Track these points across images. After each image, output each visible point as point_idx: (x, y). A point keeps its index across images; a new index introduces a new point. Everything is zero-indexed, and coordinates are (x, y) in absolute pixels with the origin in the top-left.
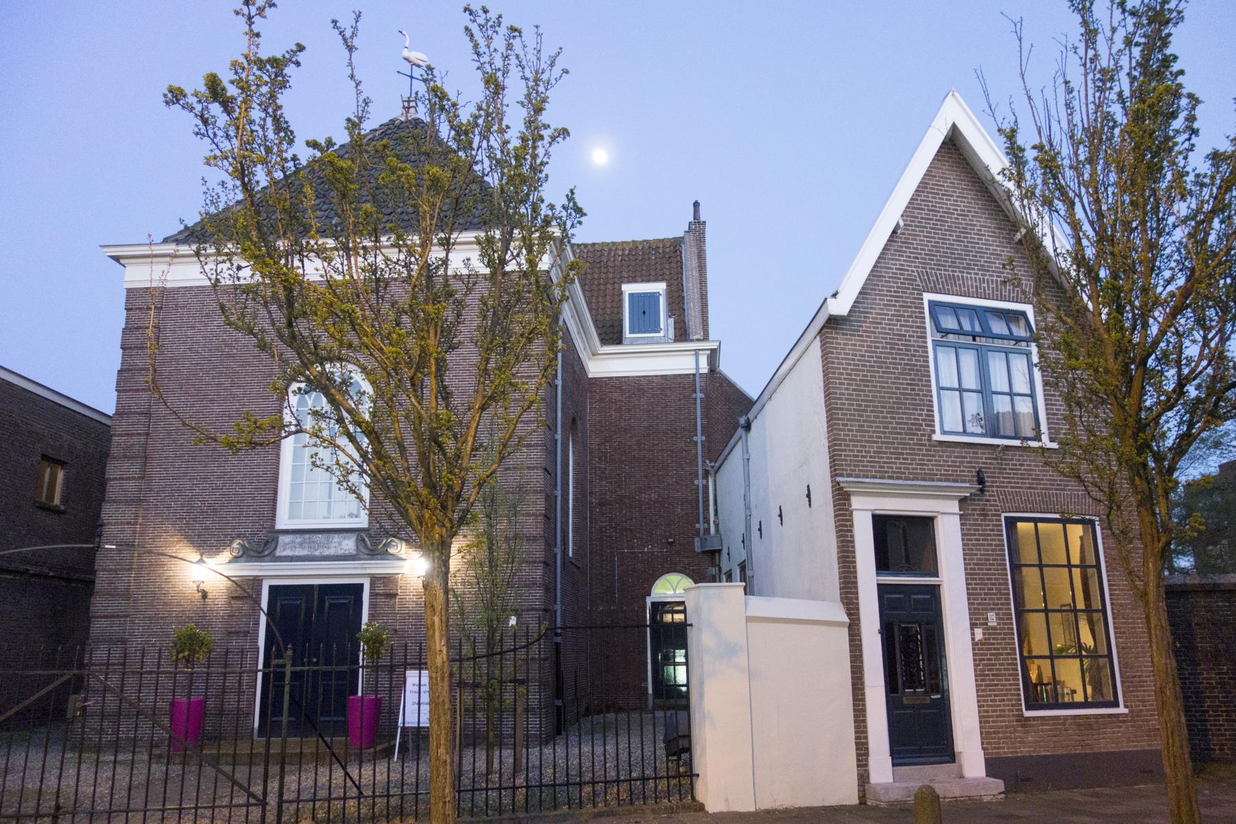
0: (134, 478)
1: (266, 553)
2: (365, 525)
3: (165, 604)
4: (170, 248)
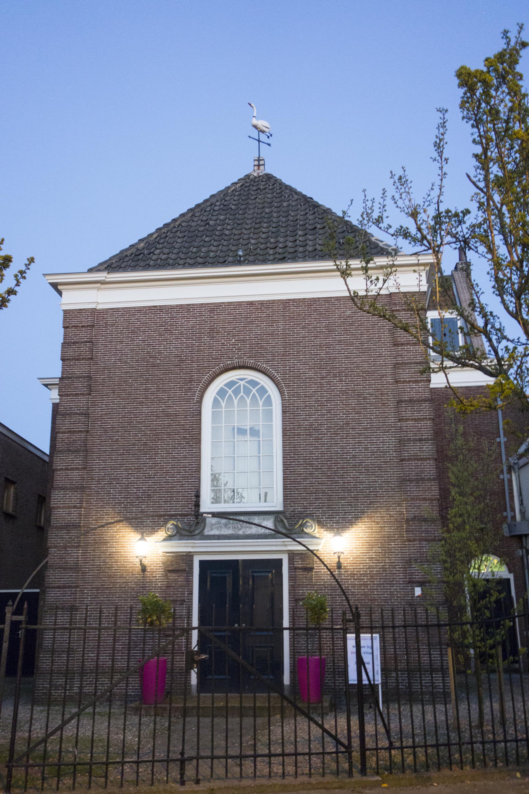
0: (77, 469)
1: (197, 532)
2: (279, 507)
3: (110, 577)
4: (102, 276)
